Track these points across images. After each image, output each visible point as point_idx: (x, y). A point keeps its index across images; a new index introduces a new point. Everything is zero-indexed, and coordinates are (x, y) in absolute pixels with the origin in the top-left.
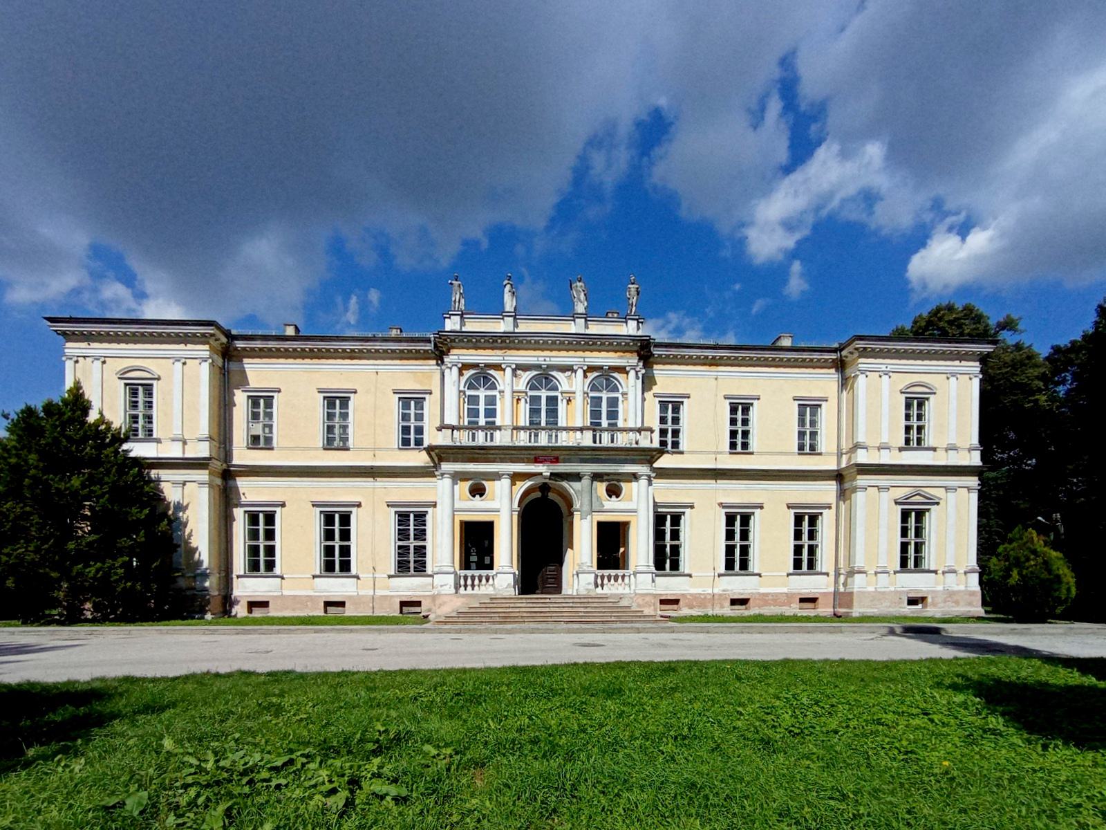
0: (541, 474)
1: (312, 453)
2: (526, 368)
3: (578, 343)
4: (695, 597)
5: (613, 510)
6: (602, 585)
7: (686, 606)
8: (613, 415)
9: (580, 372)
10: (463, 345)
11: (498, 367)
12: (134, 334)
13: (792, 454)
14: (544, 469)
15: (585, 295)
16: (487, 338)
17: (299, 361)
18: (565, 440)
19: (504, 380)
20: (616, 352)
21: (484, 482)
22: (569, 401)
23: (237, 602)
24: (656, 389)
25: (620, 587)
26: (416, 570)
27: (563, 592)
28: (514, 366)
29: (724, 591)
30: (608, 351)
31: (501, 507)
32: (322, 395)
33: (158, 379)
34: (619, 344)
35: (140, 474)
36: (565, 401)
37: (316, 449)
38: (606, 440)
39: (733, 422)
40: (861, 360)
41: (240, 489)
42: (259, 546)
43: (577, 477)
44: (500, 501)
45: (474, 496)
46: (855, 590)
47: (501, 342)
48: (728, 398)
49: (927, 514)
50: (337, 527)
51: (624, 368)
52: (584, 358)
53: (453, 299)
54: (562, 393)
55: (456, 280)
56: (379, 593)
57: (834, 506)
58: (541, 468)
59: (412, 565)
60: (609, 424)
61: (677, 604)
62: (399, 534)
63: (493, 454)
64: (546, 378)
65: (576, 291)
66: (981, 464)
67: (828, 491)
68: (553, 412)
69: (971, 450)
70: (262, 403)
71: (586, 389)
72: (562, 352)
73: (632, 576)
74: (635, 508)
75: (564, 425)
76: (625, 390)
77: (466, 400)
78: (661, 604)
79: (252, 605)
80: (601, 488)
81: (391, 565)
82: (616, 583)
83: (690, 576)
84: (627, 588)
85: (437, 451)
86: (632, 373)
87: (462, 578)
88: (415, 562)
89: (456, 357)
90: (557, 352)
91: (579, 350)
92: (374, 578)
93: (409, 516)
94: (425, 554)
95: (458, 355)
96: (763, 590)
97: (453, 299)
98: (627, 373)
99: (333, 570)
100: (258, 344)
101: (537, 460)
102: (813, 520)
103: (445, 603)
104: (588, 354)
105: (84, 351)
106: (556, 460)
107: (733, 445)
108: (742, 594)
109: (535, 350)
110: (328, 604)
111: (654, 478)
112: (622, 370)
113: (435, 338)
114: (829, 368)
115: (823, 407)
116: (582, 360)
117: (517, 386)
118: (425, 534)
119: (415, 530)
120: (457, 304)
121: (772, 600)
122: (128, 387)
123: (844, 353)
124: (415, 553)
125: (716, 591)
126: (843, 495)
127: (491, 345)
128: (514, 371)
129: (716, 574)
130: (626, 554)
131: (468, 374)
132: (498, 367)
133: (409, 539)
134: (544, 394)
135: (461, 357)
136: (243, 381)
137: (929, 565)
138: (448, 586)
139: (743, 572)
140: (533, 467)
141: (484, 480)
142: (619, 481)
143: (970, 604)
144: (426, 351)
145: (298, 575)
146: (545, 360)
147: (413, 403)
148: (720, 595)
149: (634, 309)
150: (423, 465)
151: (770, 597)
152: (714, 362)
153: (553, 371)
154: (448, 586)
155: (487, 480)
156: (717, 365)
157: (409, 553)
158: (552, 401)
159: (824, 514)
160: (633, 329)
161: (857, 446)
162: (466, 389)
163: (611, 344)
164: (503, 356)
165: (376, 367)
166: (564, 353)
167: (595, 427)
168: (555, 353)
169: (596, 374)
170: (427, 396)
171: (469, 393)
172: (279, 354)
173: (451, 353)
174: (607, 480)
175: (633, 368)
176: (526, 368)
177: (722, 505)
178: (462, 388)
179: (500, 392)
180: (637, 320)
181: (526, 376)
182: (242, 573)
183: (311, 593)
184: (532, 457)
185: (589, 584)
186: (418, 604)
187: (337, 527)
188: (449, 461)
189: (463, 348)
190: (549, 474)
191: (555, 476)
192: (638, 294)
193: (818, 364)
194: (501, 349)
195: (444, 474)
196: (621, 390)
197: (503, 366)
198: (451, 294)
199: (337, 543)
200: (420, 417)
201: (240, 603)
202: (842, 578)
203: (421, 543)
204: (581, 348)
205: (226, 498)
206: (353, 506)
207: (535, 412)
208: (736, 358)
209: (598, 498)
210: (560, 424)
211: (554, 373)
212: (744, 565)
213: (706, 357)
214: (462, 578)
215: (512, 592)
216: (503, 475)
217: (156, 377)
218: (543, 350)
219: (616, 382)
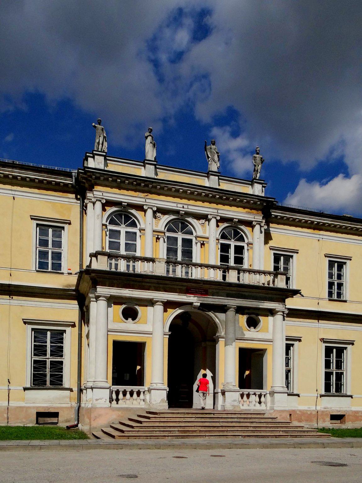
0: (191, 304)
2: (165, 212)
3: (214, 197)
4: (303, 413)
5: (253, 338)
6: (117, 400)
7: (296, 420)
8: (239, 260)
9: (213, 222)
10: (107, 183)
11: (140, 208)
15: (218, 156)
16: (131, 181)
18: (197, 274)
19: (147, 222)
20: (244, 208)
21: (137, 307)
22: (203, 244)
24: (271, 243)
25: (135, 402)
26: (52, 383)
27: (194, 406)
28: (155, 209)
31: (153, 328)
32: (35, 222)
34: (248, 202)
36: (199, 244)
38: (232, 277)
39: (331, 276)
43: (223, 309)
44: (153, 325)
45: (127, 319)
47: (144, 186)
51: (252, 222)
52: (218, 209)
53: (97, 141)
54: (196, 237)
55: (100, 124)
56: (13, 404)
57: (77, 324)
58: (192, 298)
59: (48, 378)
60: (221, 264)
62: (35, 350)
63: (133, 281)
64: (182, 223)
65: (211, 152)
67: (68, 310)
68: (188, 253)
71: (218, 236)
72: (198, 202)
73: (268, 395)
75: (199, 262)
76: (250, 240)
77: (108, 233)
80: (243, 319)
81: (26, 376)
82: (131, 398)
83: (298, 395)
85: (93, 275)
86: (257, 228)
87: (114, 393)
88: (51, 376)
89: (101, 194)
90: (229, 207)
91: (220, 204)
92: (9, 390)
94: (62, 368)
95: (101, 192)
96: (354, 409)
97: (97, 141)
98: (145, 211)
101: (187, 291)
103: (100, 415)
104: (220, 206)
108: (339, 411)
110: (40, 415)
111: (286, 317)
112: (249, 224)
113: (78, 173)
116: (216, 211)
117: (157, 226)
118: (62, 351)
119: (51, 346)
120: (100, 146)
124: (51, 368)
125: (318, 408)
127: (134, 188)
128: (155, 212)
129: (319, 395)
130: (142, 371)
131: (110, 210)
132: (140, 208)
133: (46, 355)
134: (180, 236)
135: (104, 194)
139: (338, 394)
141: (137, 305)
142: (258, 315)
144: (66, 185)
147: (50, 230)
148: (323, 412)
149: (258, 175)
150: (62, 288)
154: (104, 400)
155: (140, 305)
156: (320, 230)
157: (46, 368)
158: (187, 243)
159: (348, 349)
160: (259, 191)
162: (107, 224)
163: (241, 201)
164: (146, 199)
165: (13, 193)
167: (226, 270)
168: (192, 202)
169: (226, 225)
170: (66, 226)
171: (168, 234)
172: (24, 183)
173: (95, 189)
175: (259, 223)
176: (165, 212)
177: (323, 340)
178: (104, 222)
179: (140, 230)
180: (155, 165)
183: (22, 404)
185: (234, 401)
186: (56, 415)
190: (199, 304)
191: (205, 307)
192: (262, 163)
193: (329, 228)
194: (143, 192)
195: (99, 297)
196: (138, 228)
197: (145, 207)
198: (95, 136)
199: (49, 359)
200: (58, 244)
203: (58, 359)
204: (186, 196)
206: (68, 326)
207: (171, 251)
208: (335, 226)
209: (241, 328)
210: (194, 261)
211: (190, 219)
212: (339, 388)
213: (312, 222)
214: (114, 393)
215: (164, 406)
216: (158, 301)
218: (181, 198)
219: (242, 233)
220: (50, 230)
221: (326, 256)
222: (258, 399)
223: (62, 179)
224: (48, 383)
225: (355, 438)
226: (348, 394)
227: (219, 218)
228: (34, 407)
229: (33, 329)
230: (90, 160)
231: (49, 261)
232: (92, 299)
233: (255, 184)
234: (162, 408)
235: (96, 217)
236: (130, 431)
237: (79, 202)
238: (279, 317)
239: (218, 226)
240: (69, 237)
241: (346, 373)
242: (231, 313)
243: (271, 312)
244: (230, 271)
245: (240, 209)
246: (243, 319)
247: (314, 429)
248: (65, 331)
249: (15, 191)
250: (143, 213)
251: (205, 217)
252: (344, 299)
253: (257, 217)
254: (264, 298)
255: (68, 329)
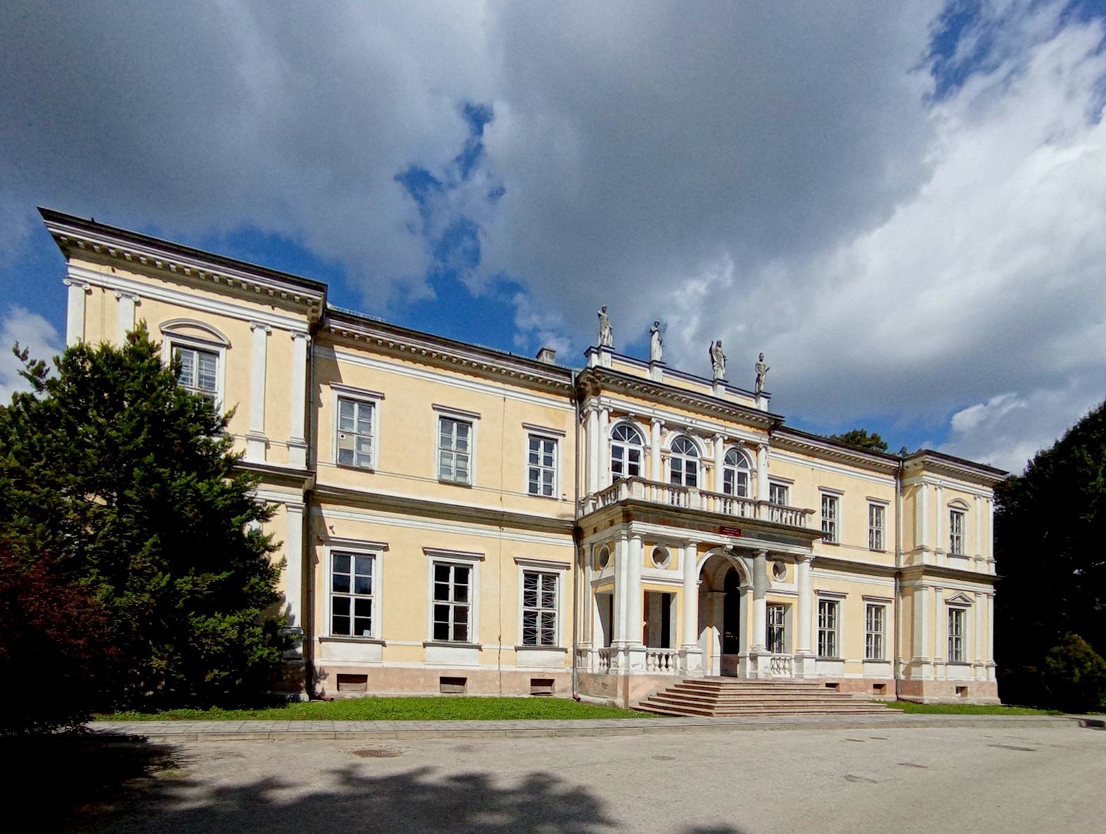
0: (721, 546)
1: (424, 485)
11: (647, 420)
12: (195, 274)
13: (863, 549)
14: (727, 541)
16: (641, 386)
17: (408, 363)
20: (751, 426)
21: (668, 548)
23: (324, 675)
29: (819, 675)
30: (745, 425)
31: (684, 573)
32: (438, 414)
33: (228, 347)
35: (239, 489)
36: (704, 469)
37: (430, 480)
39: (534, 458)
40: (925, 472)
41: (326, 520)
42: (349, 599)
43: (753, 553)
44: (685, 571)
46: (924, 679)
48: (527, 428)
49: (962, 614)
50: (451, 583)
52: (726, 427)
56: (505, 668)
57: (572, 566)
58: (725, 539)
61: (551, 685)
63: (684, 518)
64: (687, 442)
66: (995, 574)
67: (885, 587)
69: (989, 562)
70: (360, 403)
72: (638, 400)
74: (796, 590)
76: (755, 467)
78: (532, 685)
79: (343, 679)
80: (770, 565)
84: (788, 673)
90: (687, 412)
93: (536, 577)
95: (612, 399)
96: (847, 676)
99: (446, 637)
100: (361, 331)
101: (722, 531)
102: (550, 579)
105: (105, 279)
106: (738, 533)
107: (533, 488)
109: (682, 409)
110: (535, 682)
112: (754, 446)
114: (890, 475)
115: (790, 489)
121: (855, 685)
122: (174, 349)
123: (906, 464)
126: (901, 590)
132: (647, 420)
134: (684, 458)
135: (612, 401)
136: (333, 376)
137: (838, 654)
138: (640, 666)
139: (338, 636)
140: (718, 538)
141: (668, 545)
142: (783, 562)
143: (992, 694)
144: (563, 386)
145: (398, 645)
146: (691, 422)
150: (555, 518)
151: (853, 683)
152: (811, 453)
153: (694, 435)
154: (640, 666)
155: (671, 547)
156: (814, 456)
161: (922, 549)
166: (707, 418)
168: (699, 416)
170: (378, 401)
173: (601, 394)
174: (774, 560)
181: (672, 435)
182: (326, 635)
184: (718, 526)
185: (766, 667)
187: (451, 583)
188: (683, 527)
189: (614, 391)
190: (732, 547)
191: (738, 551)
199: (539, 608)
201: (330, 676)
202: (902, 668)
205: (313, 534)
216: (692, 542)
217: (226, 343)
218: (689, 411)
219: (745, 457)
220: (455, 425)
221: (820, 489)
222: (657, 662)
223: (560, 378)
224: (539, 641)
225: (126, 722)
226: (561, 646)
227: (611, 410)
228: (528, 673)
229: (332, 551)
230: (594, 356)
231: (540, 482)
232: (623, 537)
233: (762, 398)
234: (698, 676)
235: (601, 428)
236: (689, 701)
237: (574, 408)
238: (806, 565)
239: (610, 421)
240: (563, 452)
241: (839, 631)
242: (761, 559)
243: (797, 559)
244: (762, 506)
245: (747, 428)
246: (770, 565)
247: (869, 701)
248: (558, 574)
249: (478, 384)
250: (649, 427)
251: (711, 436)
252: (836, 542)
253: (761, 438)
254: (789, 538)
255: (563, 572)
